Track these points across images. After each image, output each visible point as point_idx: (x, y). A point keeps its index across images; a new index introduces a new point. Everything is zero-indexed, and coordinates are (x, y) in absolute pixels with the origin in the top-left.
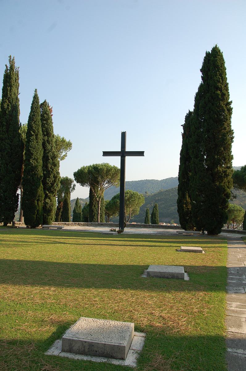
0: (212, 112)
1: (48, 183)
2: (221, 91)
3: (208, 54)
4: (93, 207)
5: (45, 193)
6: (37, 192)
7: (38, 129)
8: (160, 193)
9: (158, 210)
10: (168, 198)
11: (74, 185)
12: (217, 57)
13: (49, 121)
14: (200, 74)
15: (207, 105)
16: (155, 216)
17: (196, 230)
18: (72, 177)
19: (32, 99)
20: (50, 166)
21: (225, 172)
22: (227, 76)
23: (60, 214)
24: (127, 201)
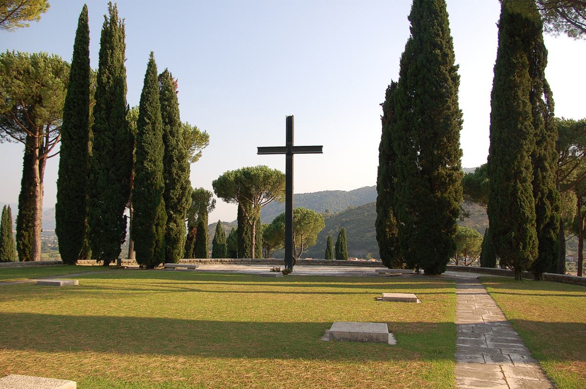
1: (173, 198)
2: (441, 50)
4: (244, 235)
5: (168, 213)
7: (156, 114)
11: (214, 201)
13: (173, 101)
14: (408, 24)
16: (342, 248)
17: (406, 268)
18: (210, 189)
19: (146, 68)
20: (174, 171)
23: (193, 246)
24: (296, 225)
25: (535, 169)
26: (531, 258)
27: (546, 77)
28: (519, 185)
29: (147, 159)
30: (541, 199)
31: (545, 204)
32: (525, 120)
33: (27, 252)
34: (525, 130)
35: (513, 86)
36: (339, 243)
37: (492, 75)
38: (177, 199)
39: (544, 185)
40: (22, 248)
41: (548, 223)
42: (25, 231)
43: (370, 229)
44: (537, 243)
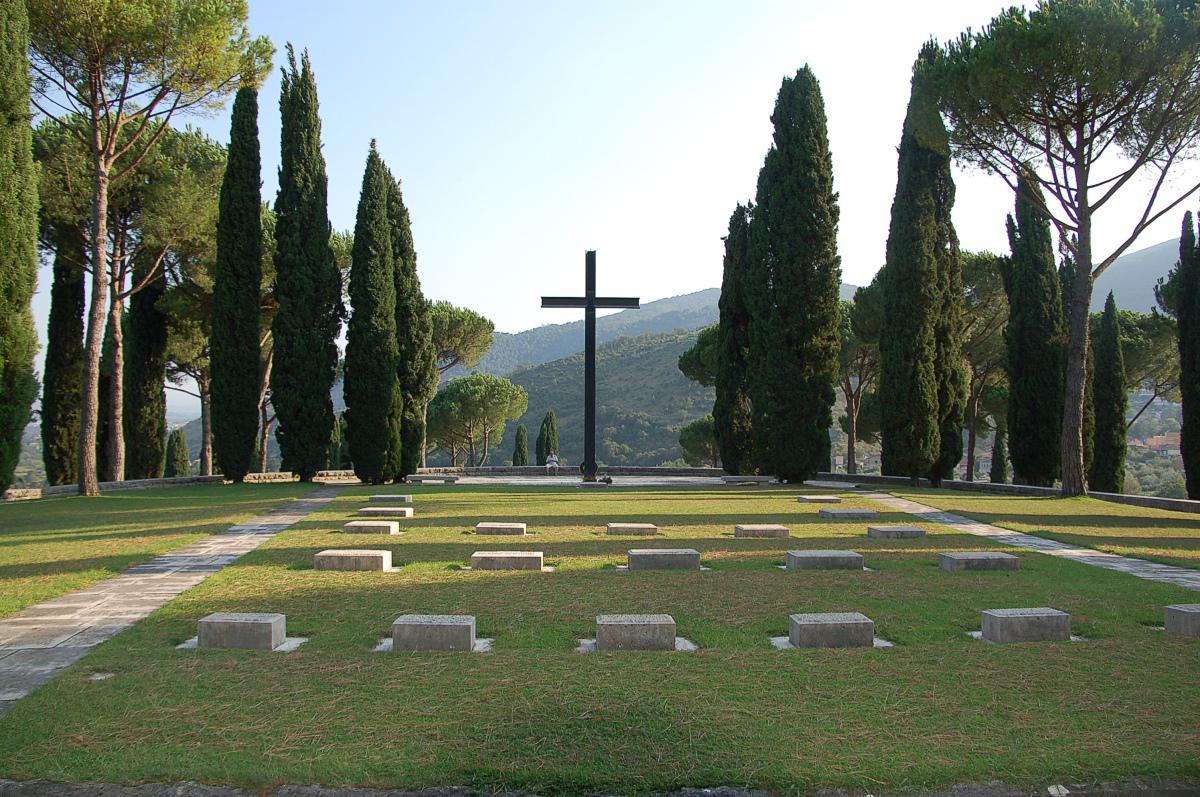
0: (799, 218)
1: (411, 374)
2: (818, 171)
3: (786, 83)
5: (404, 397)
6: (390, 396)
7: (385, 241)
8: (519, 375)
9: (555, 428)
13: (404, 218)
14: (771, 128)
15: (787, 200)
20: (414, 331)
21: (826, 348)
22: (828, 136)
25: (938, 342)
26: (932, 459)
27: (953, 220)
28: (921, 366)
29: (376, 312)
30: (943, 384)
31: (947, 389)
32: (929, 281)
35: (917, 237)
36: (543, 439)
37: (888, 218)
38: (417, 374)
40: (57, 458)
41: (951, 415)
42: (61, 426)
43: (564, 411)
44: (939, 438)
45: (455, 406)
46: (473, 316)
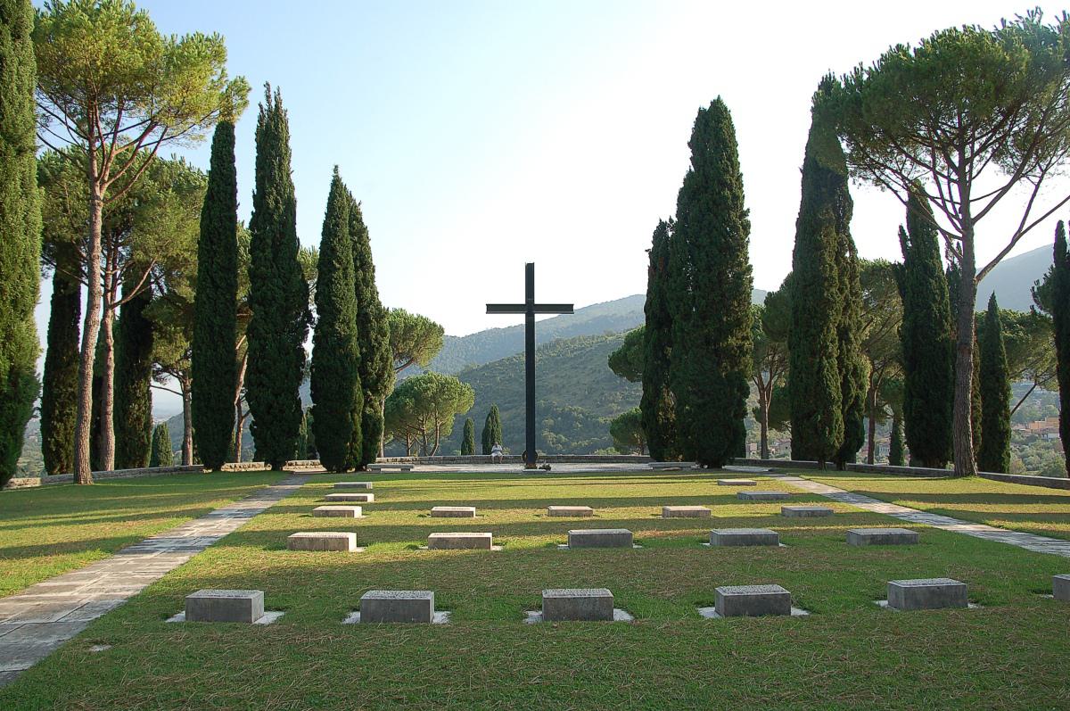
1: (371, 374)
2: (731, 190)
3: (702, 113)
5: (365, 394)
10: (491, 387)
12: (722, 123)
14: (689, 153)
17: (683, 461)
19: (329, 189)
20: (373, 335)
22: (739, 159)
24: (429, 402)
25: (840, 340)
26: (837, 445)
27: (851, 231)
31: (849, 382)
33: (63, 455)
34: (832, 299)
35: (819, 247)
37: (794, 231)
39: (848, 359)
45: (410, 402)
46: (425, 322)
